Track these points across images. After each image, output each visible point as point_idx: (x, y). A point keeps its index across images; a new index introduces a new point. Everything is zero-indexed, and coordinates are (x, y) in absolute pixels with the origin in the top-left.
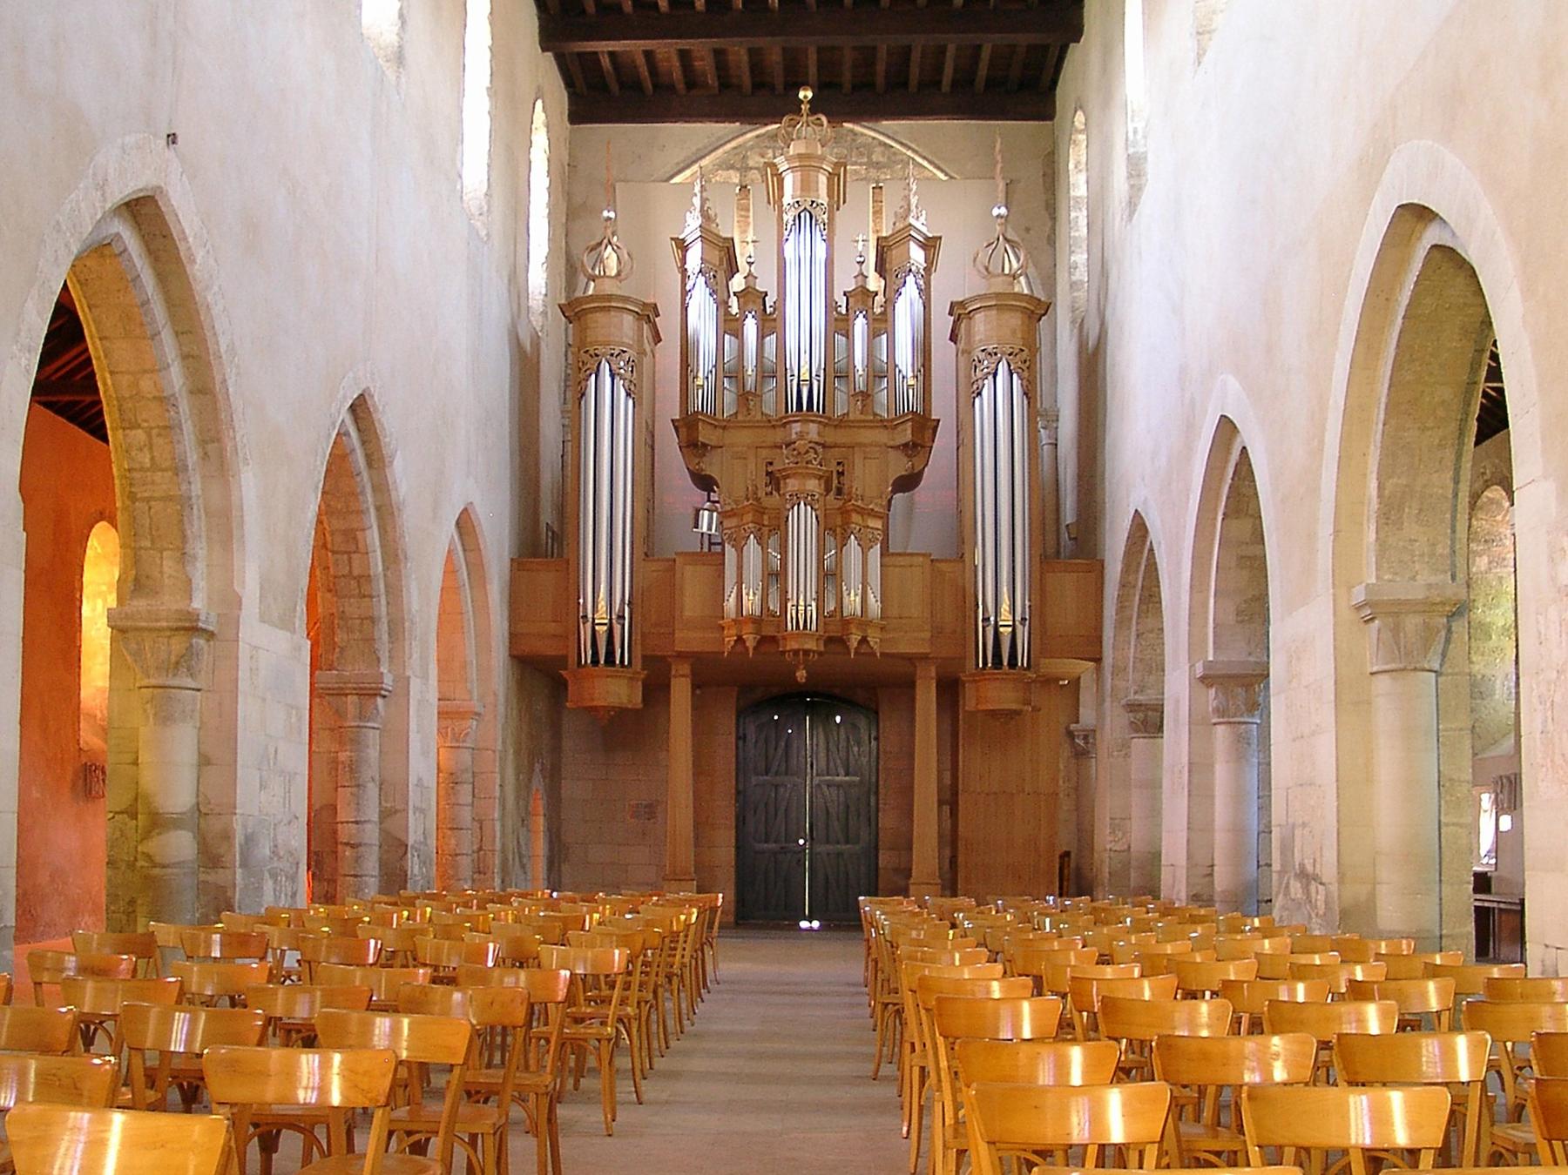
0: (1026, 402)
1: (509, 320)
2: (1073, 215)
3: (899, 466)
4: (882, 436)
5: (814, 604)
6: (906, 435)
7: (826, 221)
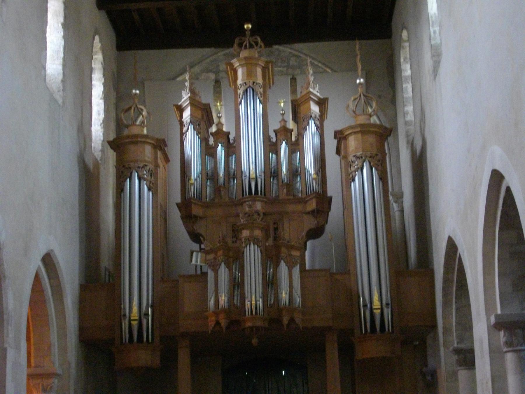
0: (381, 183)
1: (78, 150)
2: (404, 86)
3: (310, 223)
5: (261, 300)
6: (312, 205)
7: (262, 92)
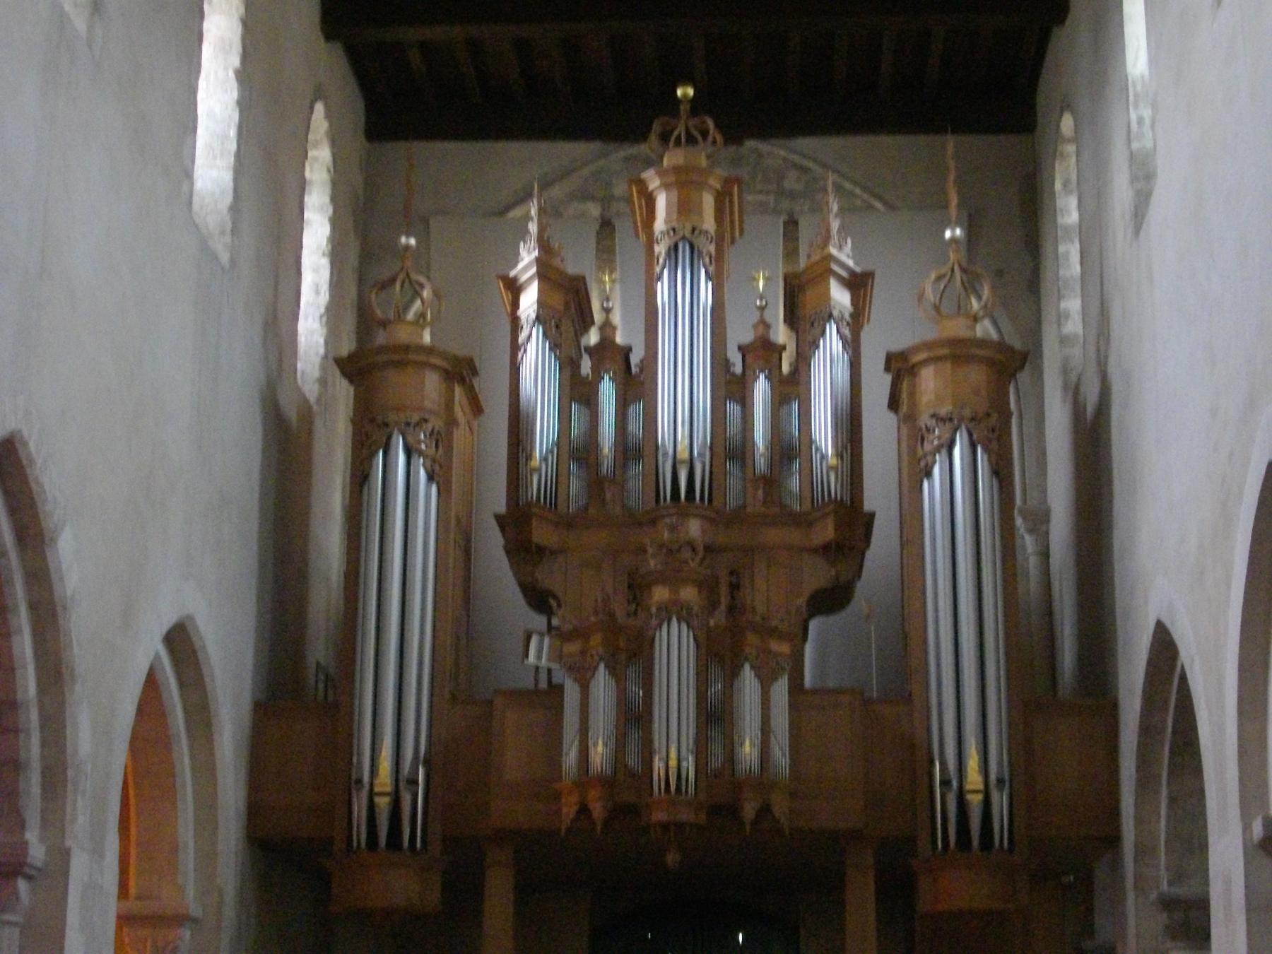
3: (817, 575)
4: (794, 536)
6: (826, 532)
7: (713, 253)
